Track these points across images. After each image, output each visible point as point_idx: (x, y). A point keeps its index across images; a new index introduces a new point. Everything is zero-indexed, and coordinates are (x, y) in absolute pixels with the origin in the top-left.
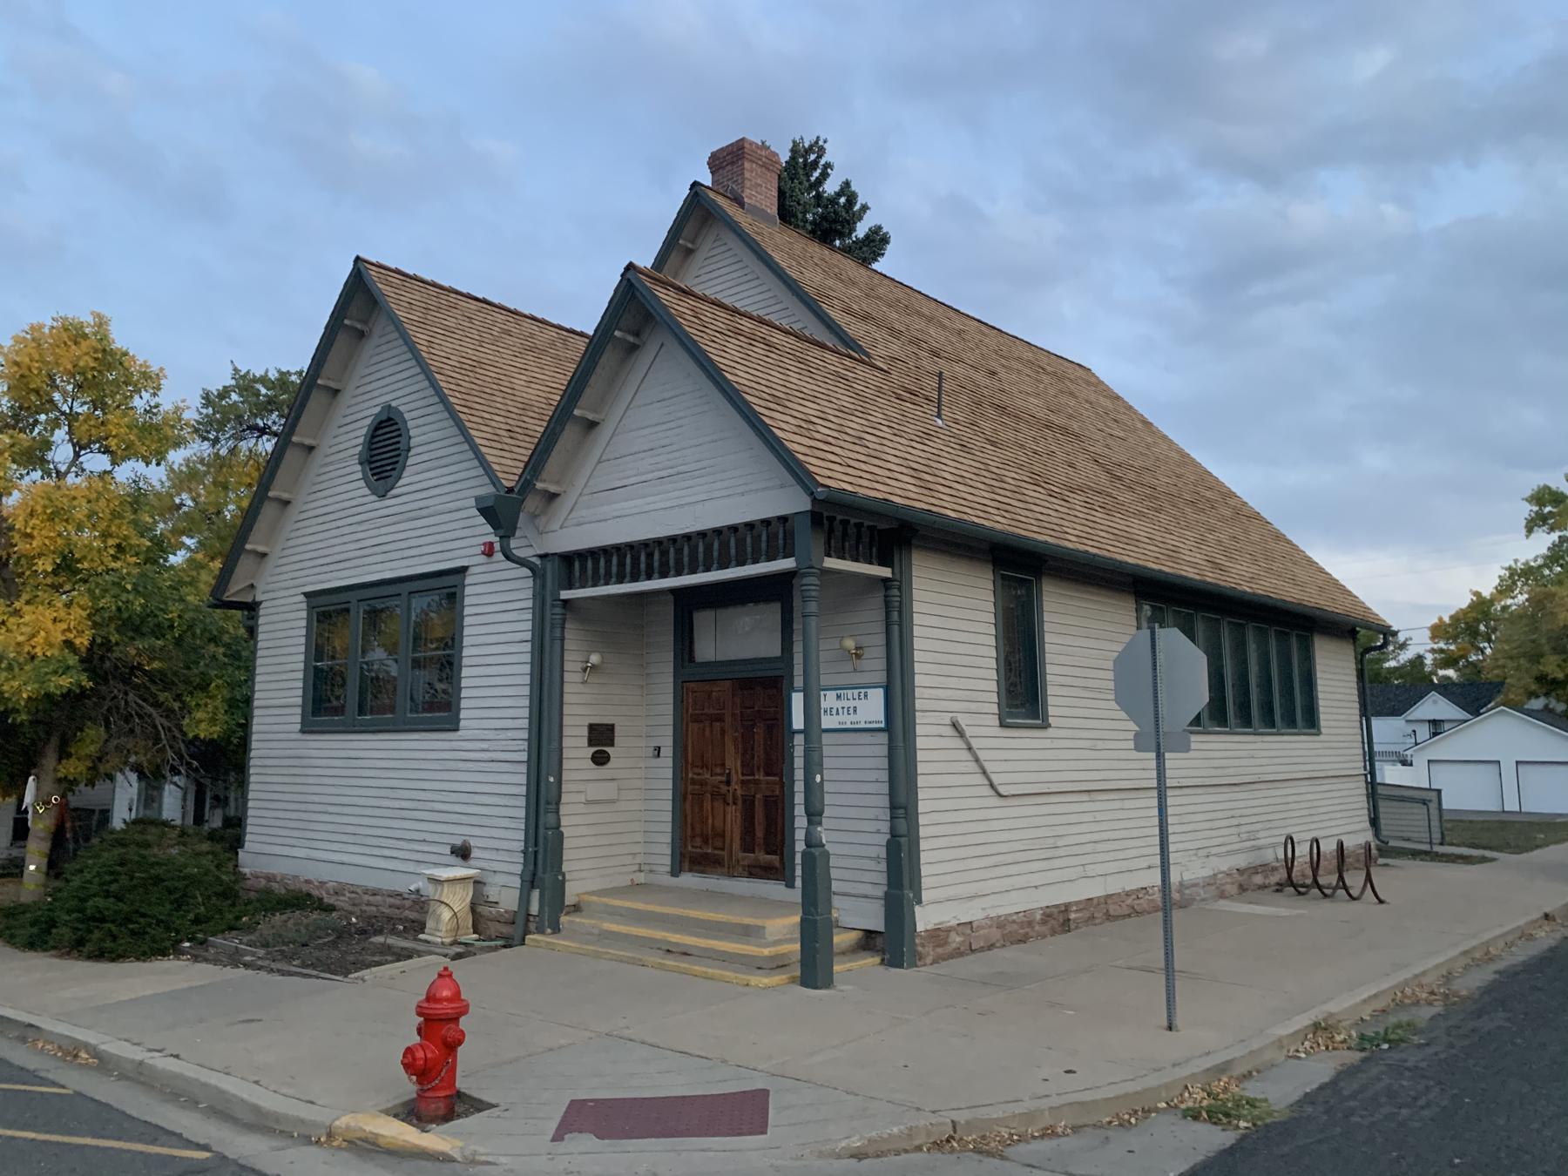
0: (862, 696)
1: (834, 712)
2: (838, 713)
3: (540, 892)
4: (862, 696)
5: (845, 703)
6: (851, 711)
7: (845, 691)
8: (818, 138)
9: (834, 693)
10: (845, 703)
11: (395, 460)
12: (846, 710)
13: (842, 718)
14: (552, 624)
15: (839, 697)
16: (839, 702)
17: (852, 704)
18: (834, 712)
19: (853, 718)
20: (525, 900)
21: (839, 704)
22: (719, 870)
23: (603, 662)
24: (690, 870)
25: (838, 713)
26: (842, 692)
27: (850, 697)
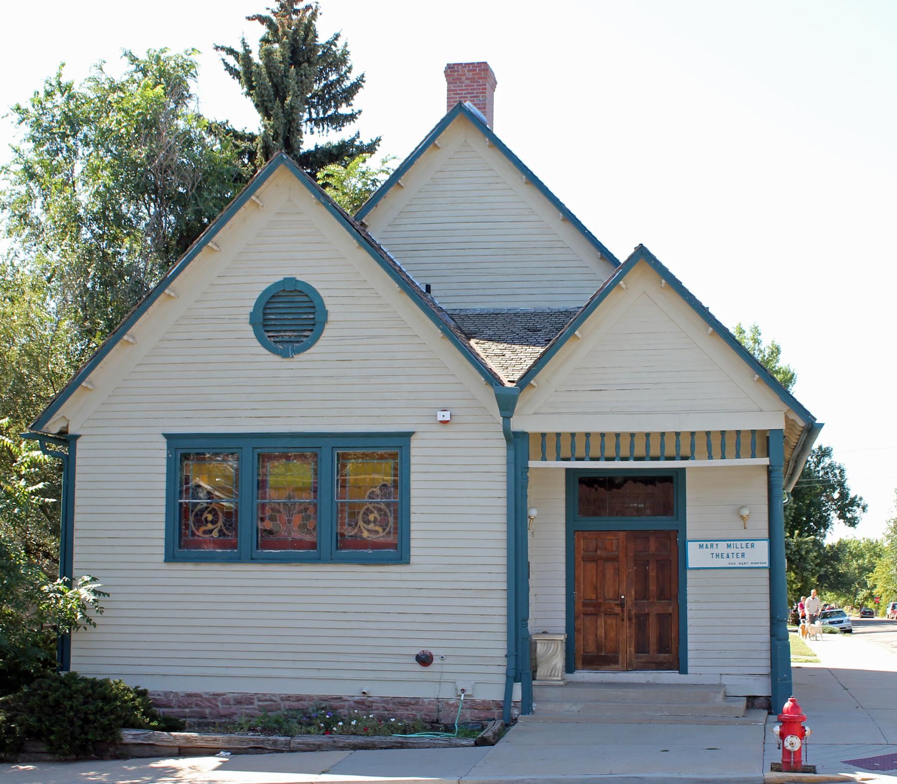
0: (749, 546)
1: (725, 556)
2: (728, 557)
3: (522, 686)
4: (749, 546)
5: (735, 551)
6: (740, 555)
7: (735, 542)
8: (337, 37)
9: (725, 543)
10: (735, 551)
11: (389, 229)
12: (735, 555)
13: (731, 560)
14: (522, 473)
15: (729, 546)
16: (729, 549)
17: (740, 551)
18: (725, 556)
19: (741, 560)
20: (508, 692)
21: (730, 551)
22: (613, 666)
23: (538, 515)
24: (583, 669)
25: (728, 557)
26: (732, 543)
27: (738, 546)
